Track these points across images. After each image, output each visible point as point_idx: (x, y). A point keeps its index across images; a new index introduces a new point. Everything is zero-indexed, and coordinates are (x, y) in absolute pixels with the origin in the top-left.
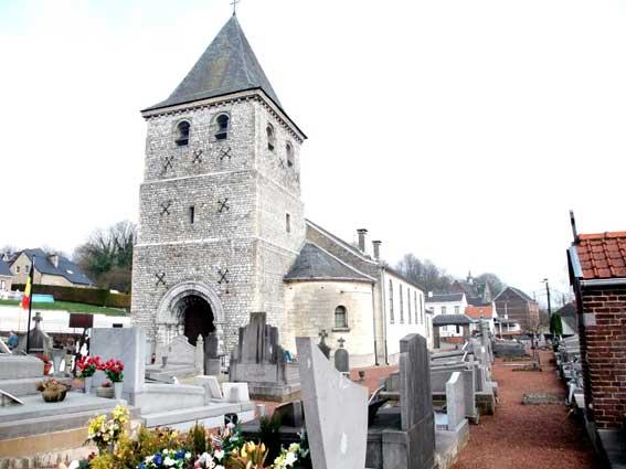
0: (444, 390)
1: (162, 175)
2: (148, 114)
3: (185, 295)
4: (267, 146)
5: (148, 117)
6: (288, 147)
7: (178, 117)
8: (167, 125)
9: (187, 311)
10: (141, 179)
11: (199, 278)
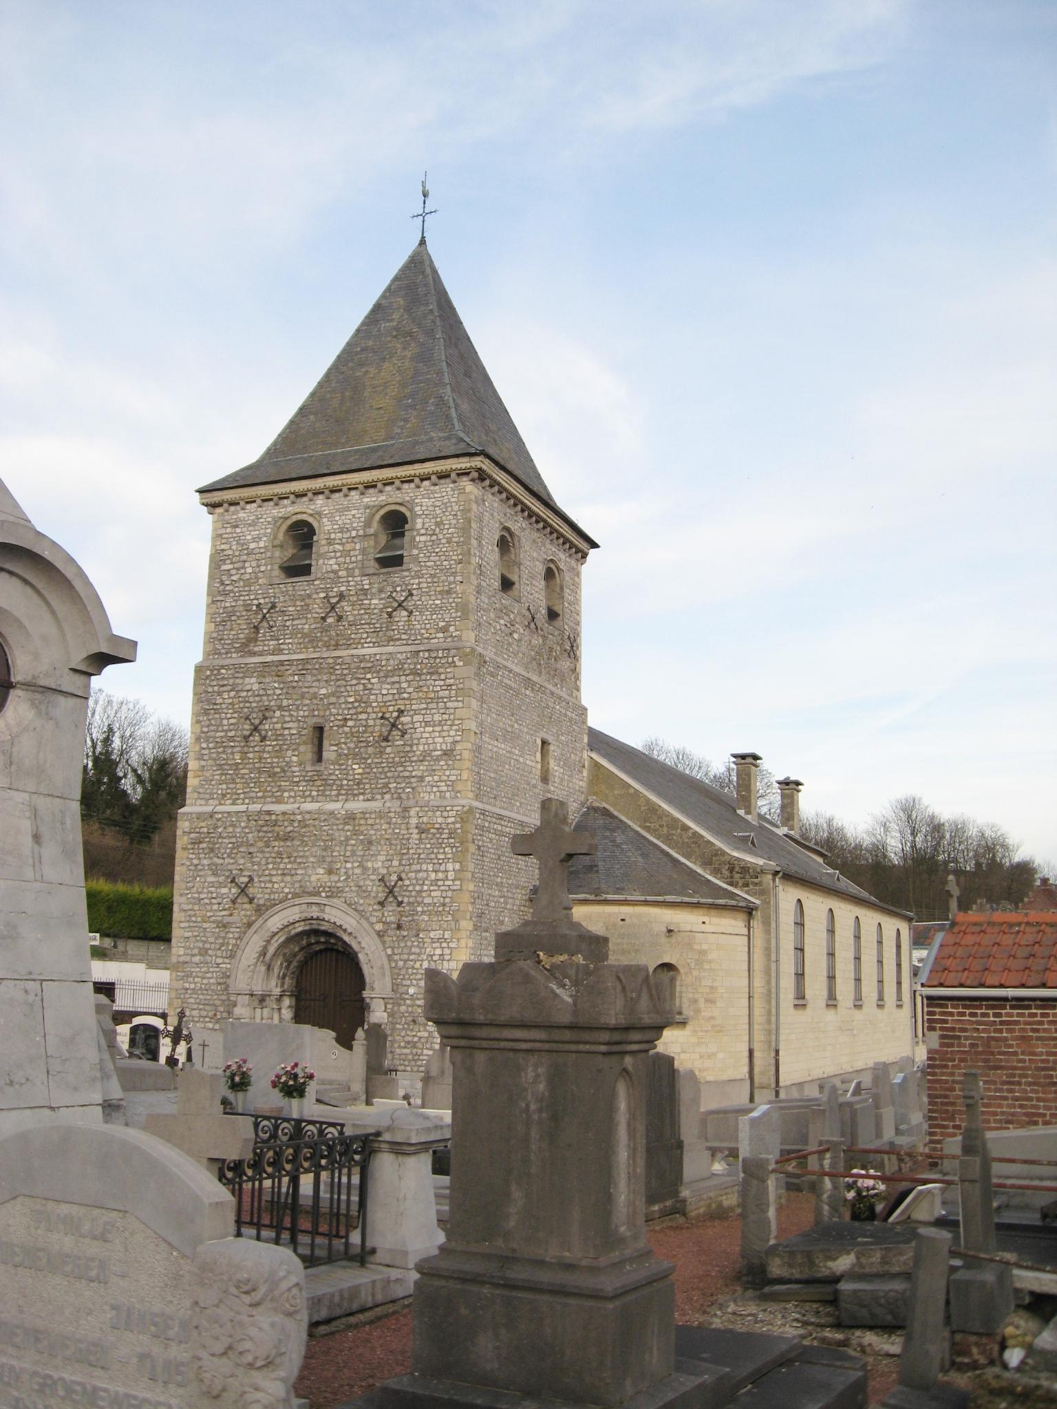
0: (737, 1140)
1: (246, 647)
2: (216, 497)
3: (300, 928)
4: (497, 584)
5: (219, 505)
6: (550, 574)
7: (289, 509)
8: (262, 525)
9: (303, 965)
10: (198, 657)
11: (333, 893)
